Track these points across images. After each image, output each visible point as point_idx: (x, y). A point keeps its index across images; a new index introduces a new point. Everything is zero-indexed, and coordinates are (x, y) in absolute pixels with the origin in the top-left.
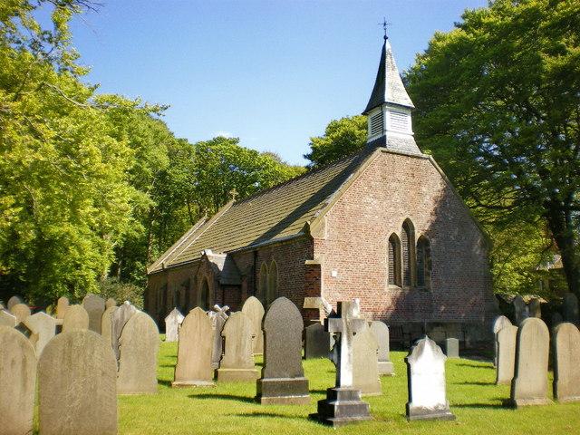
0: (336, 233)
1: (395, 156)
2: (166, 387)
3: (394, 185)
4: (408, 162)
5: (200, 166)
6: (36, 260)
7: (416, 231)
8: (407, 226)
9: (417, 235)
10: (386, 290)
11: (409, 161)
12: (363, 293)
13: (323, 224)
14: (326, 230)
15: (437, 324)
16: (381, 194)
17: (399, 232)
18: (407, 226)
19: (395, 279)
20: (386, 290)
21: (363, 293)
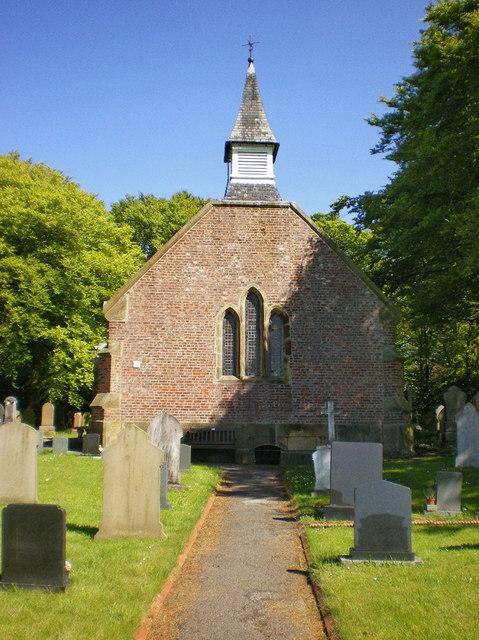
0: (142, 314)
1: (236, 210)
2: (335, 566)
3: (230, 246)
4: (256, 214)
5: (171, 205)
6: (394, 323)
7: (266, 304)
8: (254, 297)
9: (268, 309)
10: (215, 382)
11: (257, 213)
12: (178, 386)
13: (124, 304)
14: (127, 311)
15: (297, 427)
16: (211, 260)
17: (241, 306)
18: (254, 297)
19: (233, 366)
20: (215, 382)
21: (178, 386)
